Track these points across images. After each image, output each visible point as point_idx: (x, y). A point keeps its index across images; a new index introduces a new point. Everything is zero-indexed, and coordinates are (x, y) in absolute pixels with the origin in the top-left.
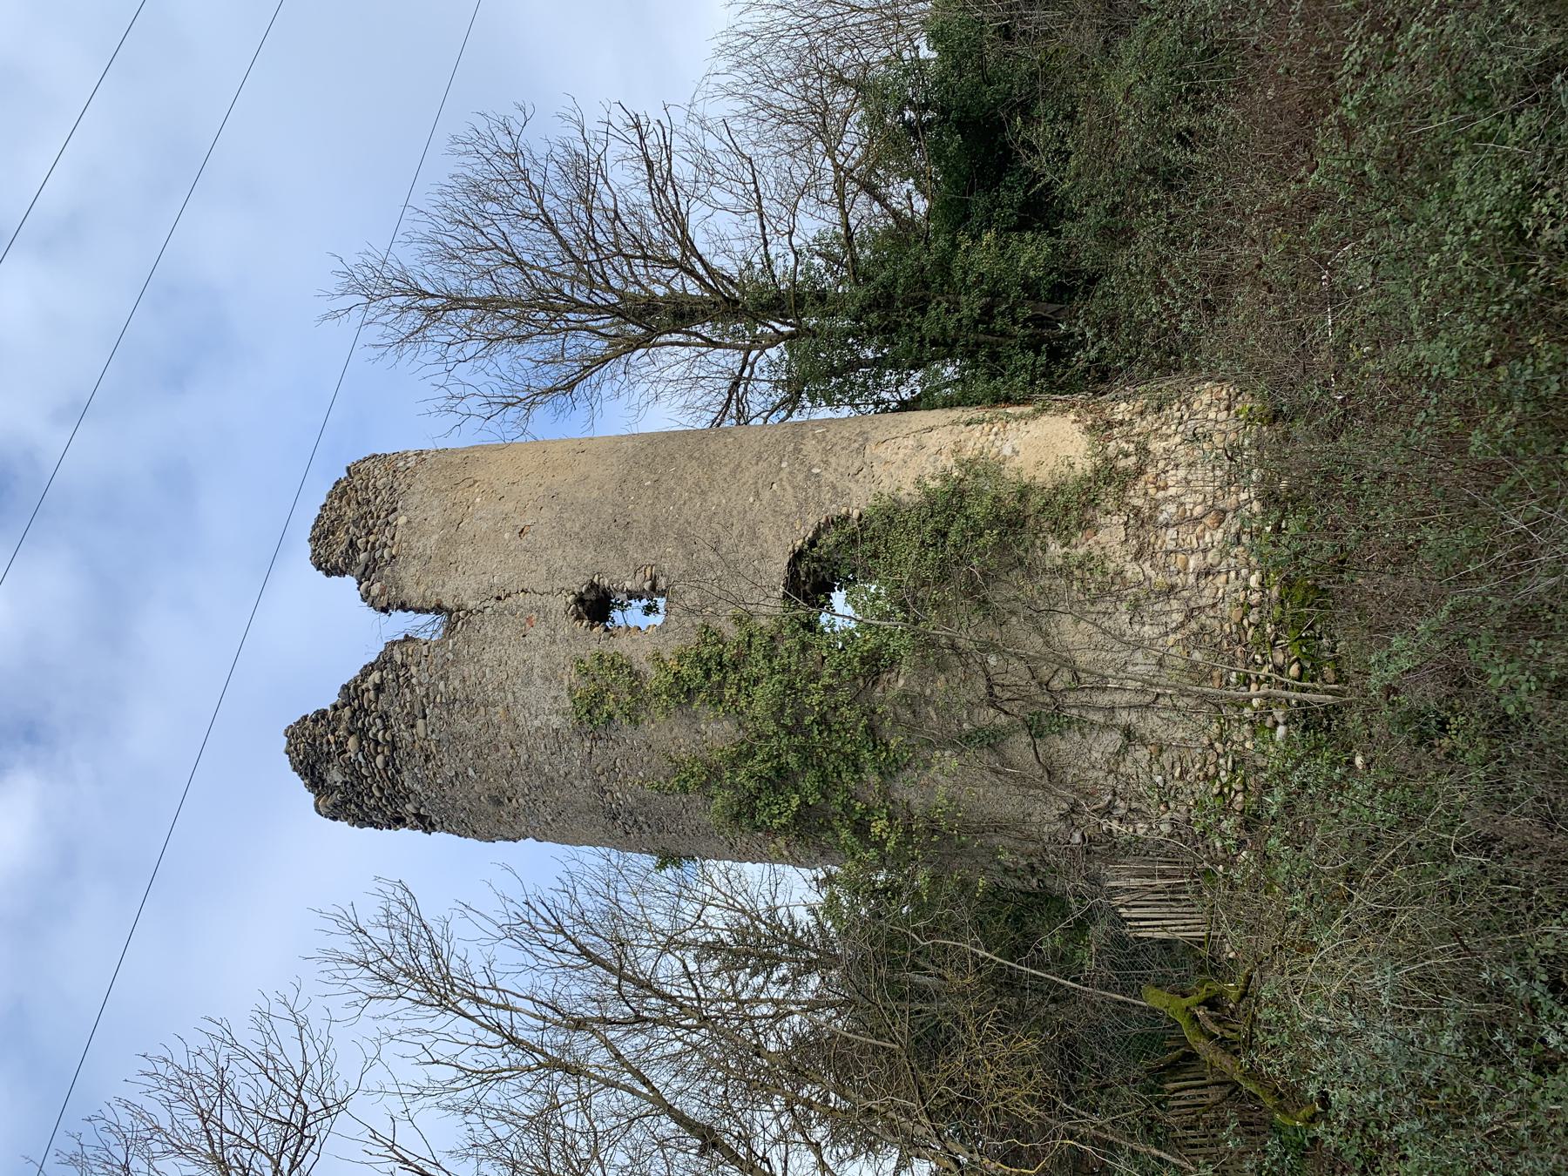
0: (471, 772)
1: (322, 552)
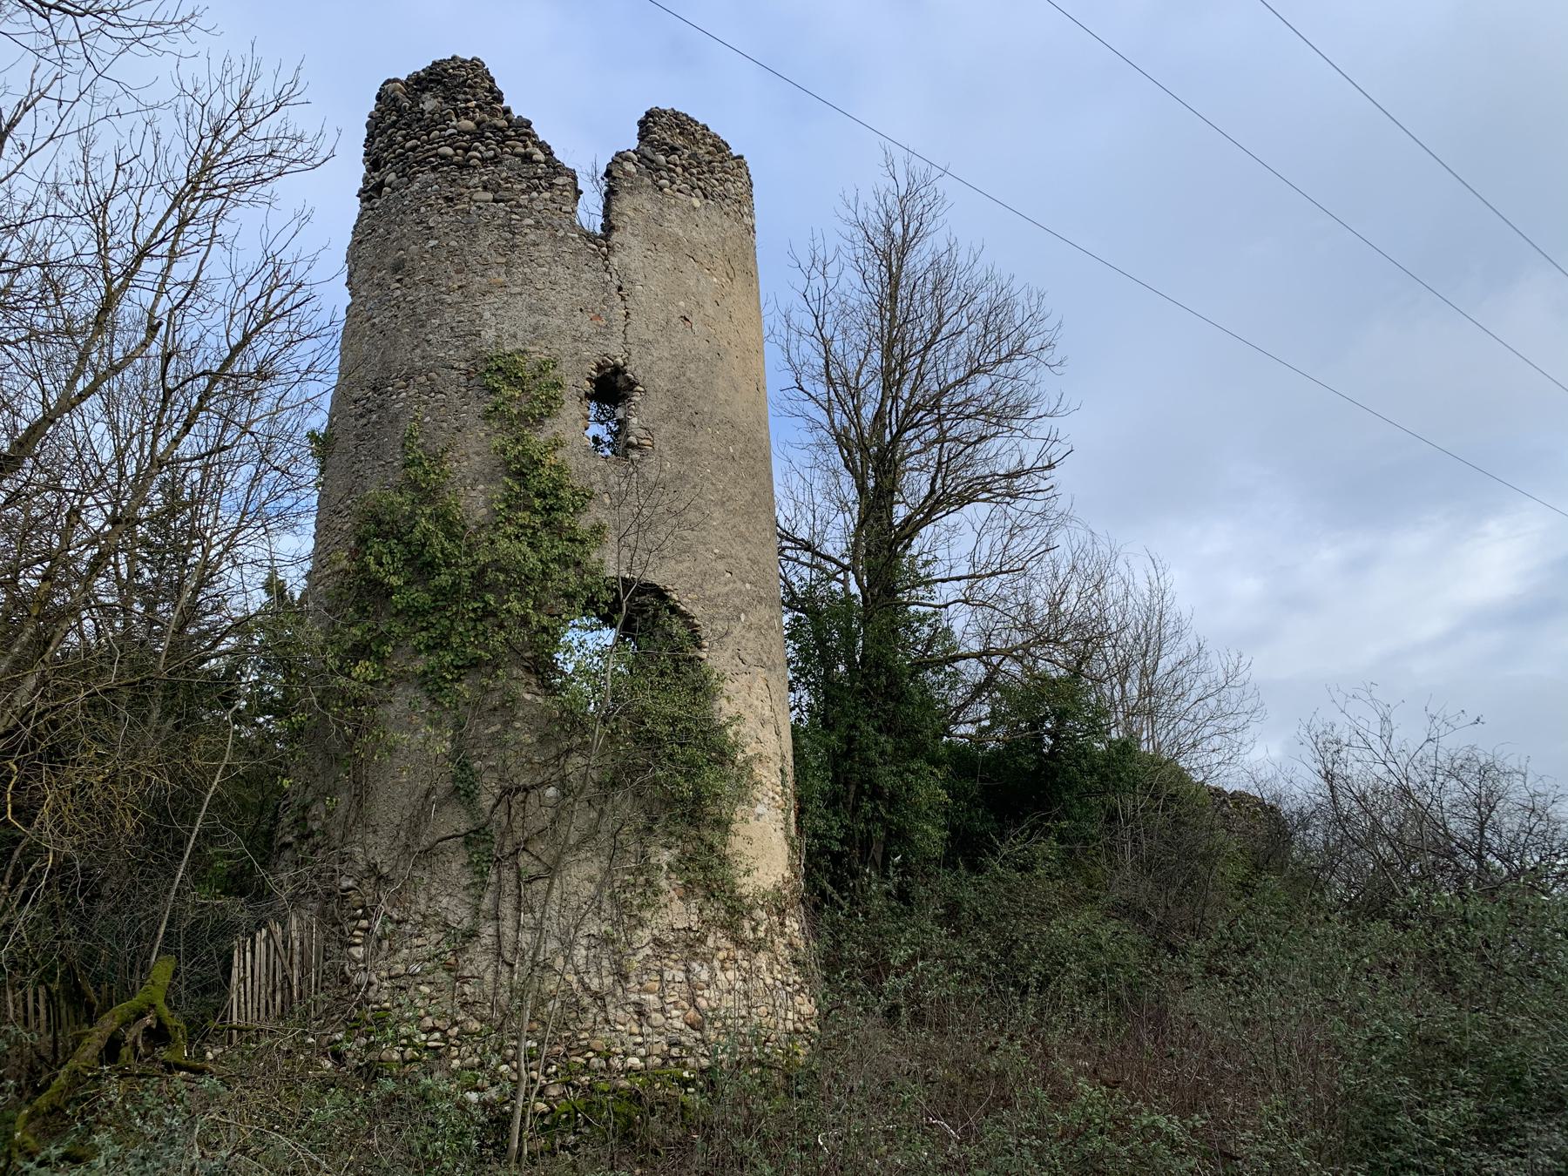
0: (433, 243)
1: (664, 120)
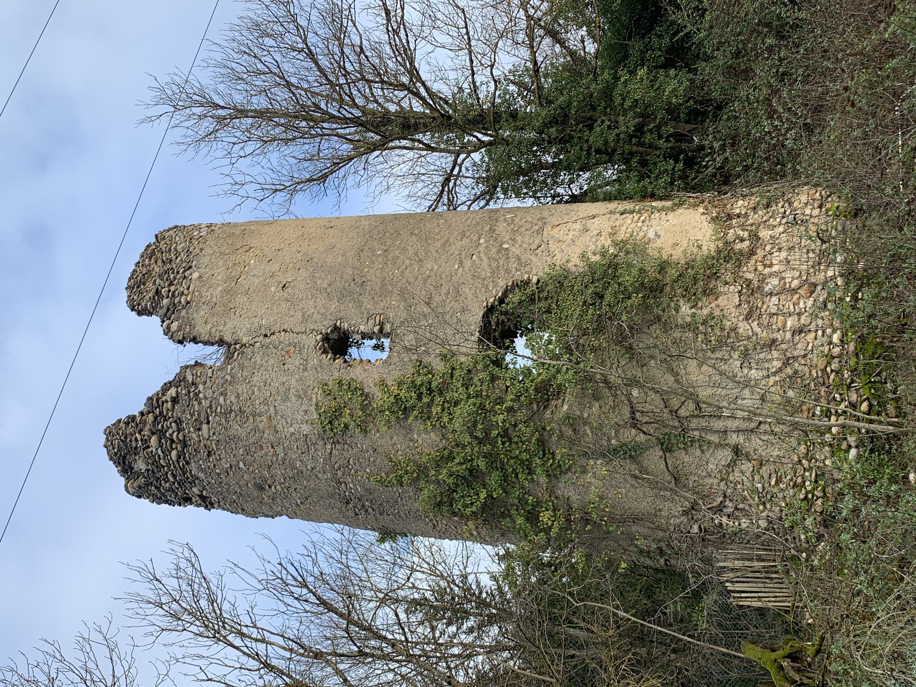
0: (241, 465)
1: (135, 297)
